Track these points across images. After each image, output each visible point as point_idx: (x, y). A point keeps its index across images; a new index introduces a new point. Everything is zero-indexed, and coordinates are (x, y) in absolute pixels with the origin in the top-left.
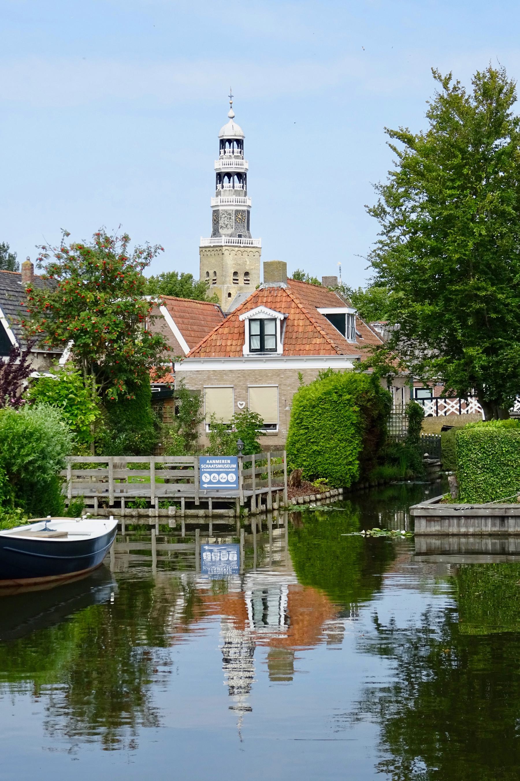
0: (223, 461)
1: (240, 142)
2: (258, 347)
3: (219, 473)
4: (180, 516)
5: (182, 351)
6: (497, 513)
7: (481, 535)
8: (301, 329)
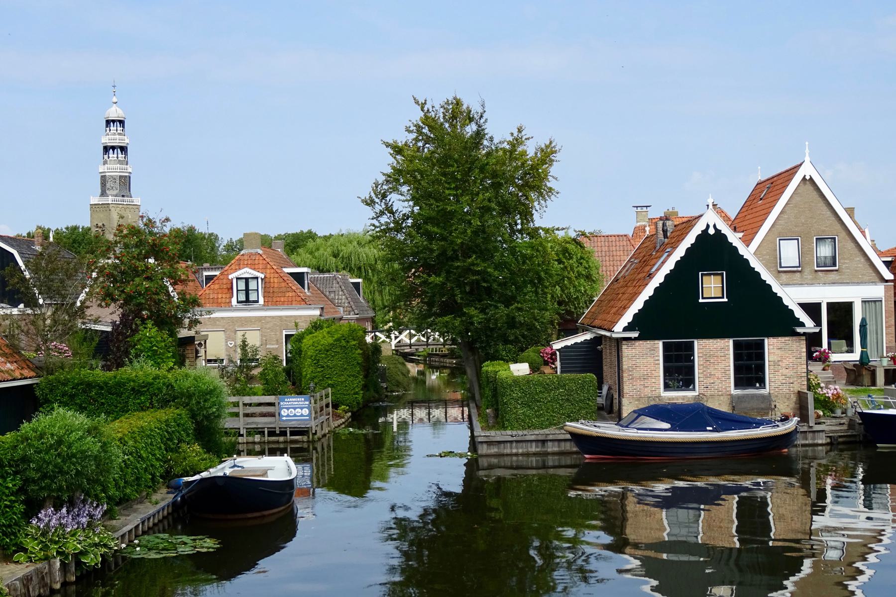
1: (122, 122)
2: (244, 299)
3: (295, 408)
4: (264, 442)
6: (540, 438)
7: (527, 455)
8: (276, 285)
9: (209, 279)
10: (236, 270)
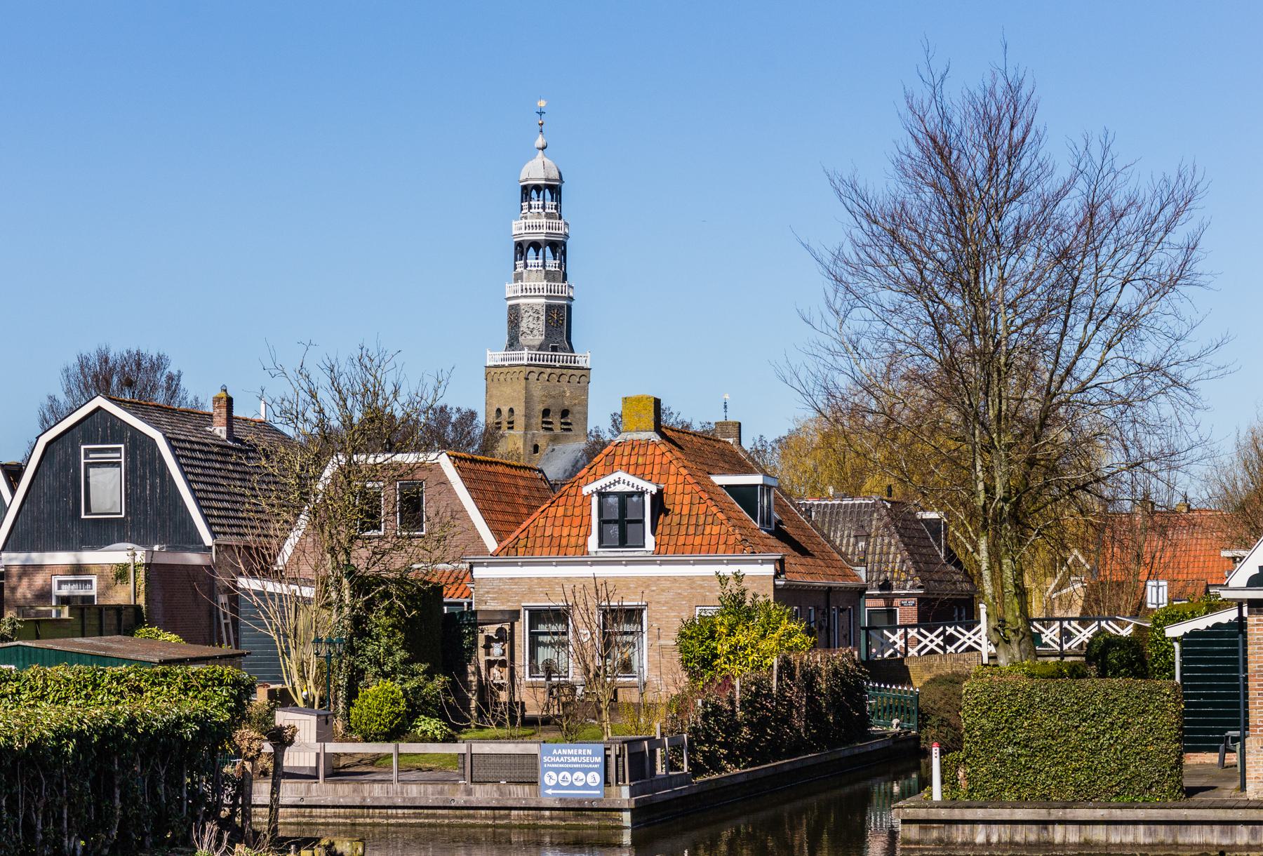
1: (555, 190)
5: (484, 545)
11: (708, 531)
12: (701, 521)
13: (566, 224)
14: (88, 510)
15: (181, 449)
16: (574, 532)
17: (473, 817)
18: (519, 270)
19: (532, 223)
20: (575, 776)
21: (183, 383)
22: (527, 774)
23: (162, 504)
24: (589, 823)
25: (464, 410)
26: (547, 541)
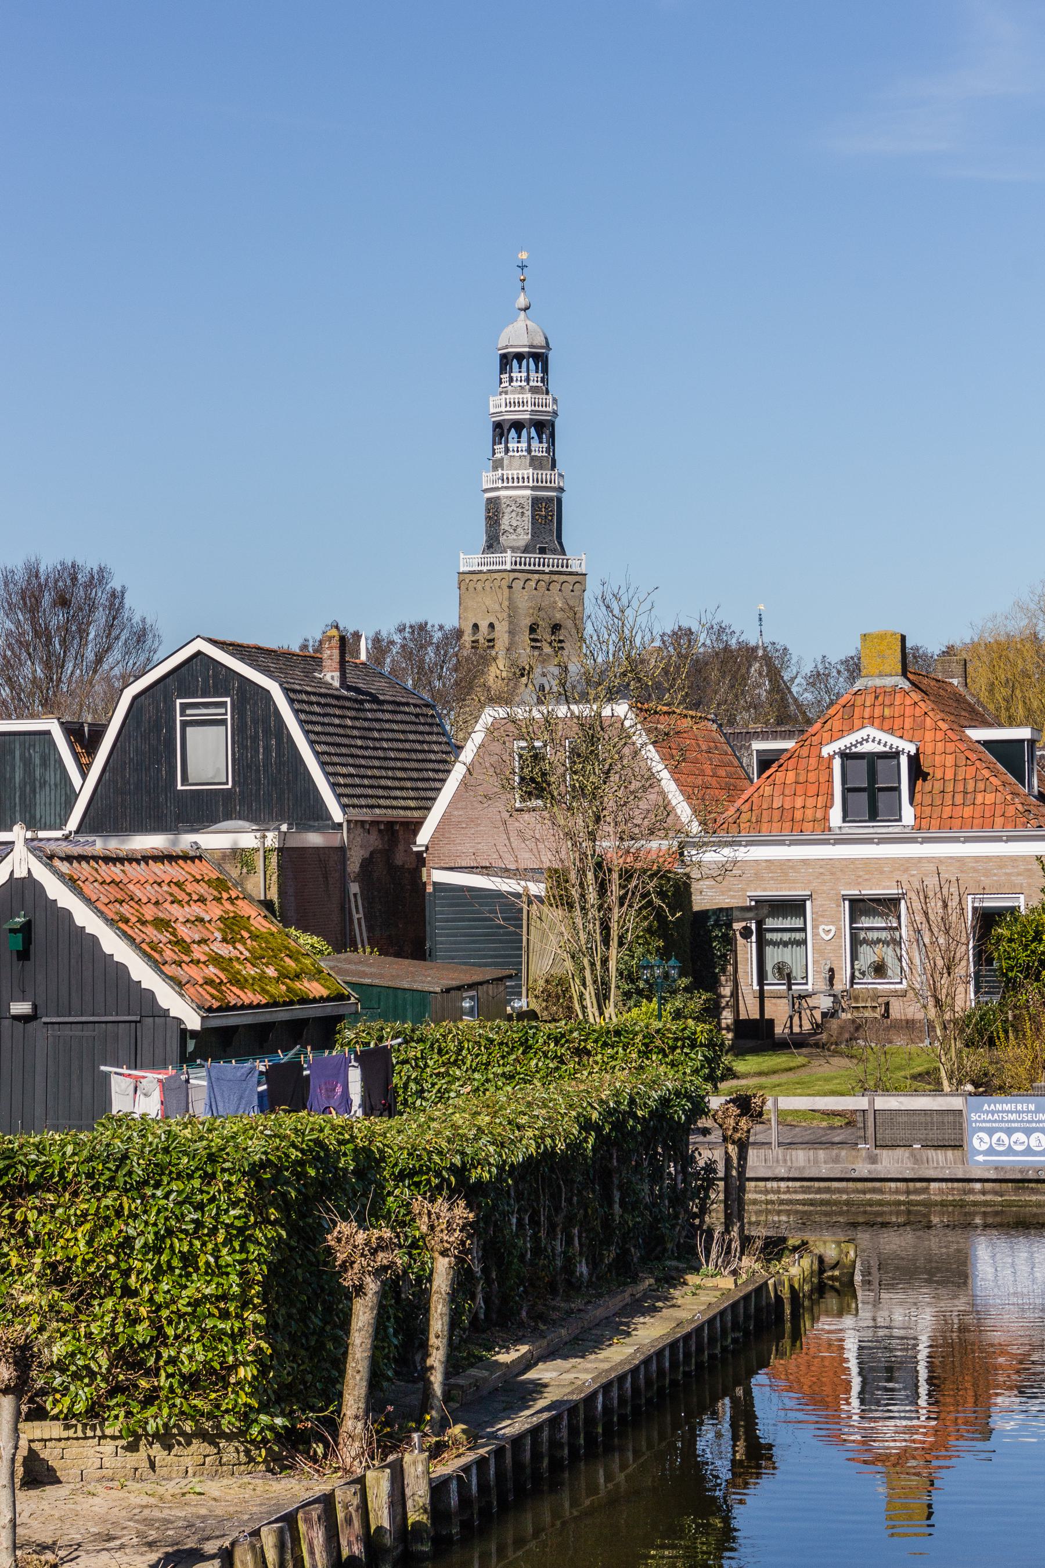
0: (1019, 1107)
1: (540, 359)
3: (1009, 1132)
9: (766, 762)
10: (842, 734)
11: (979, 799)
12: (970, 787)
13: (555, 401)
14: (185, 780)
15: (299, 701)
16: (810, 802)
17: (880, 1191)
18: (498, 456)
19: (513, 399)
20: (1014, 1137)
21: (128, 602)
22: (949, 1135)
23: (279, 771)
24: (1034, 1198)
25: (447, 628)
26: (776, 815)
